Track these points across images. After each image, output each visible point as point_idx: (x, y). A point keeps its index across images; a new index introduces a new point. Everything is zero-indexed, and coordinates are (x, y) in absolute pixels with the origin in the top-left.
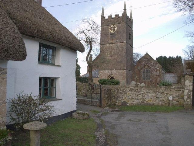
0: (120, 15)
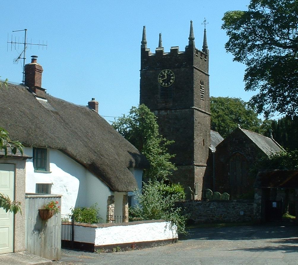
0: (182, 49)
